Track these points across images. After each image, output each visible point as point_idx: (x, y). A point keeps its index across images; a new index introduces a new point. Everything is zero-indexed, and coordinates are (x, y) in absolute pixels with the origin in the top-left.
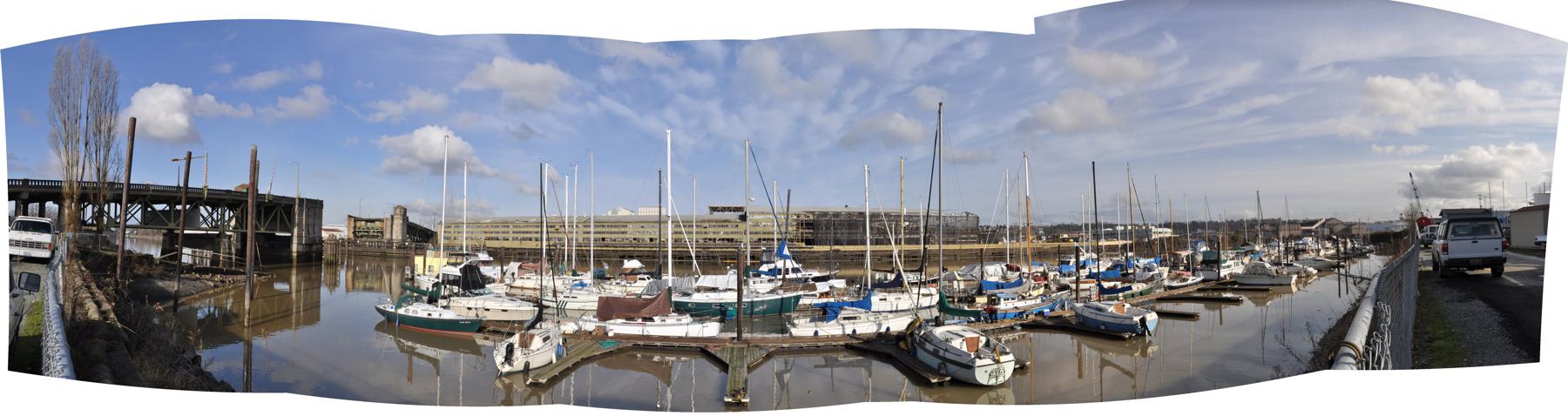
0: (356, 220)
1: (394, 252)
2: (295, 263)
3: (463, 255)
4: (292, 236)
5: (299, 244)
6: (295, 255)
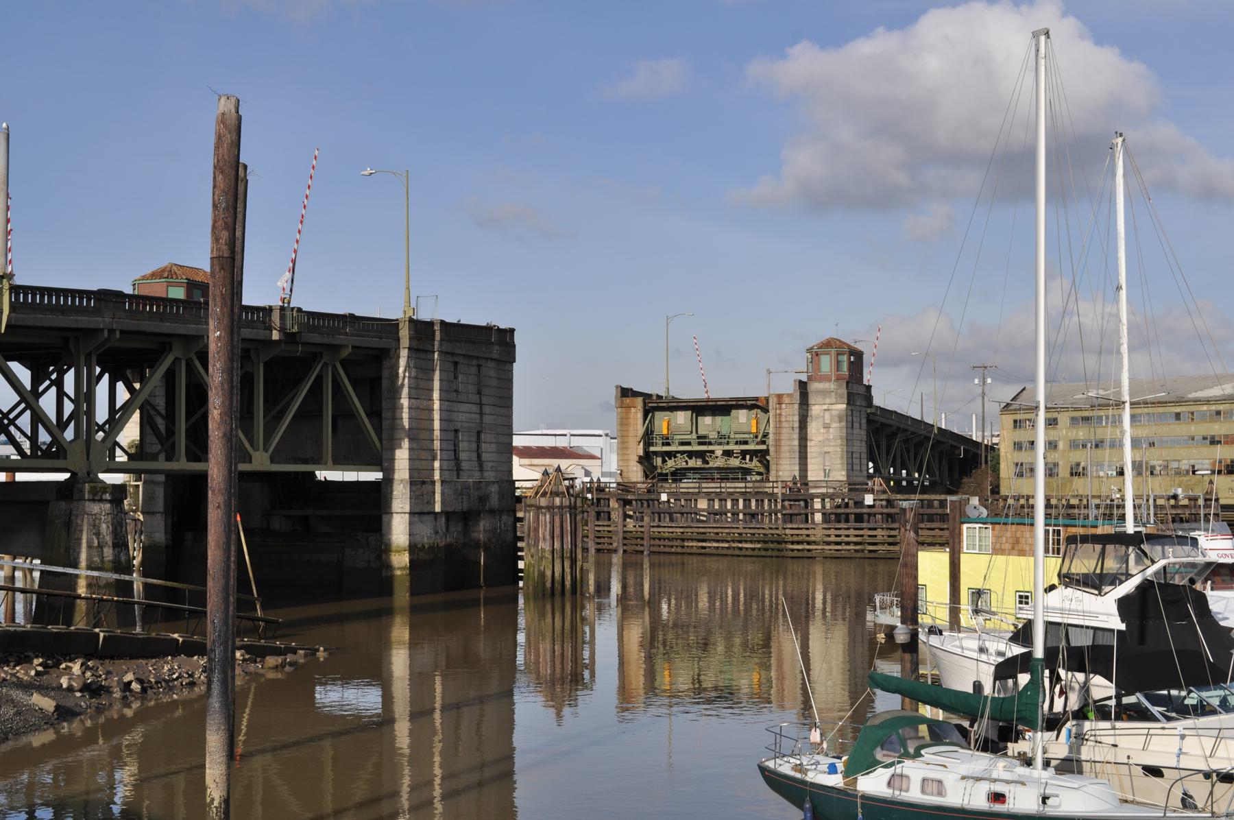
0: (653, 405)
1: (818, 534)
2: (402, 596)
3: (1122, 539)
4: (388, 481)
5: (418, 513)
6: (400, 560)
